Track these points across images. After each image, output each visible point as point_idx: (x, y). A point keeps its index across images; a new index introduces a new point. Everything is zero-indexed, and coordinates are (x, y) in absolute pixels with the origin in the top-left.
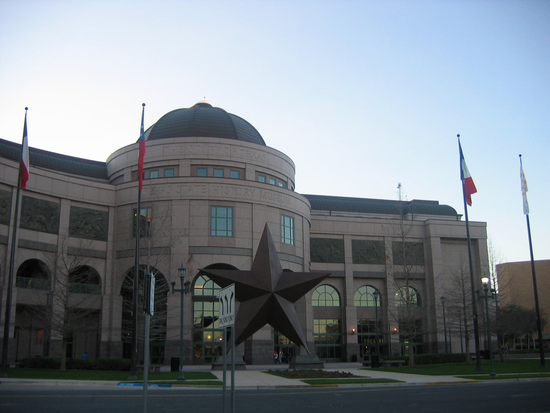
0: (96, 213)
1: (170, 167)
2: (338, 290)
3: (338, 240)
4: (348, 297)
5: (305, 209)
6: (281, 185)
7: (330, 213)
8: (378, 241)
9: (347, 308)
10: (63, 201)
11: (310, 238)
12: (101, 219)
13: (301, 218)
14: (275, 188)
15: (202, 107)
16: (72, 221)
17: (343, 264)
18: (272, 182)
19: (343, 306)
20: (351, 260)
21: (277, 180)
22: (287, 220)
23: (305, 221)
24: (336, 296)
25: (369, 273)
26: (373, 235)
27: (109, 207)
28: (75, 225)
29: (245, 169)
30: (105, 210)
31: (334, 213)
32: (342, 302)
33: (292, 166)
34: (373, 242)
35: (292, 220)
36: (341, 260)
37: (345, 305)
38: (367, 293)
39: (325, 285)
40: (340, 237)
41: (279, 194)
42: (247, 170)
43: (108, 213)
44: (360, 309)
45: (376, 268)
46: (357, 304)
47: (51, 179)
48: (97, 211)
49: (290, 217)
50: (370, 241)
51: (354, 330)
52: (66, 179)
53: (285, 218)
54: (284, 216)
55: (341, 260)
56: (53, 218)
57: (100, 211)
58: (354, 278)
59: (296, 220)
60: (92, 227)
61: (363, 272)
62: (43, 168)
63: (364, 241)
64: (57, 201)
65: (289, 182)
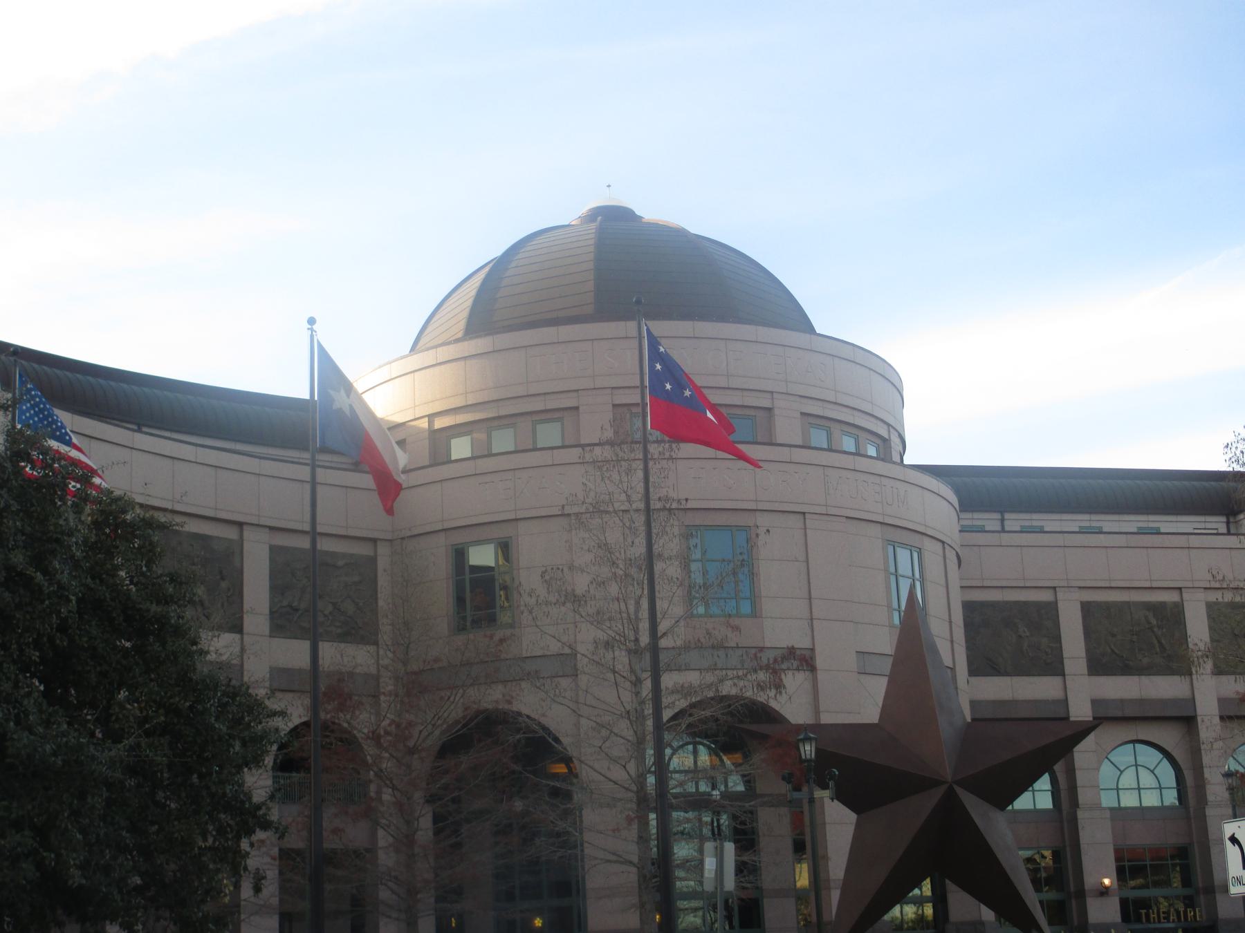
0: (340, 563)
1: (549, 416)
2: (1175, 754)
3: (1039, 606)
4: (1081, 778)
5: (939, 512)
6: (872, 451)
7: (1003, 520)
8: (1163, 605)
9: (1081, 814)
10: (248, 533)
11: (968, 607)
12: (356, 579)
13: (940, 544)
14: (862, 464)
15: (613, 223)
16: (278, 588)
17: (1058, 679)
18: (848, 444)
19: (1065, 805)
20: (1082, 666)
21: (862, 435)
22: (903, 555)
23: (951, 556)
24: (1167, 774)
25: (1141, 702)
26: (1147, 584)
27: (374, 541)
28: (285, 603)
29: (769, 410)
30: (363, 550)
31: (1014, 521)
32: (1064, 795)
33: (897, 388)
34: (1149, 606)
35: (915, 555)
36: (1053, 666)
37: (1075, 803)
38: (1136, 765)
39: (1134, 742)
40: (1046, 597)
41: (877, 480)
42: (777, 412)
43: (373, 560)
44: (1119, 814)
45: (1164, 687)
46: (1108, 800)
47: (169, 461)
48: (344, 555)
49: (910, 548)
50: (1136, 604)
51: (1107, 882)
52: (268, 467)
53: (898, 550)
54: (894, 544)
55: (1053, 666)
56: (224, 585)
57: (352, 555)
58: (1222, 718)
59: (926, 555)
60: (334, 604)
61: (1035, 703)
62: (239, 447)
63: (1115, 604)
64: (231, 533)
65: (895, 439)
